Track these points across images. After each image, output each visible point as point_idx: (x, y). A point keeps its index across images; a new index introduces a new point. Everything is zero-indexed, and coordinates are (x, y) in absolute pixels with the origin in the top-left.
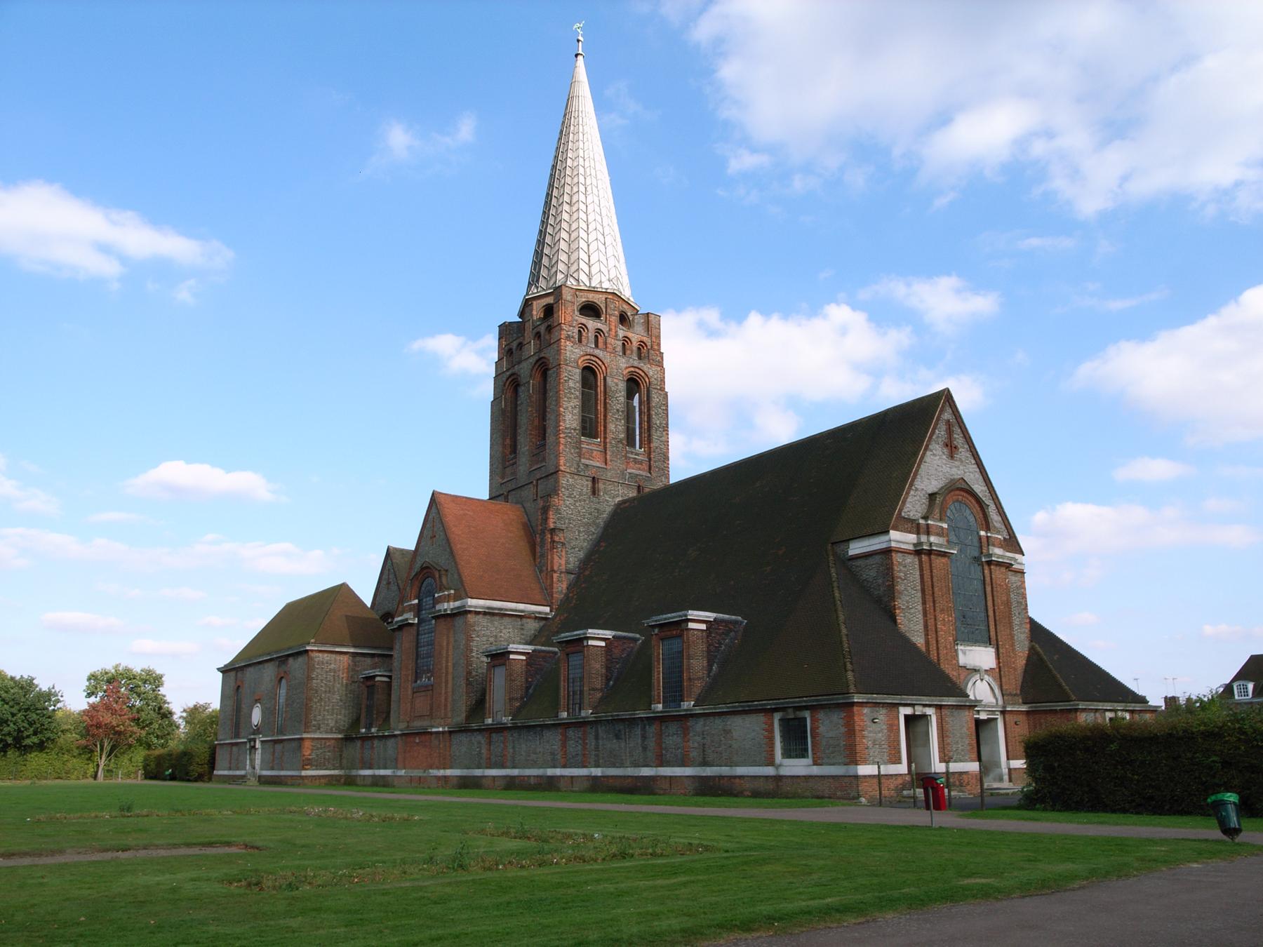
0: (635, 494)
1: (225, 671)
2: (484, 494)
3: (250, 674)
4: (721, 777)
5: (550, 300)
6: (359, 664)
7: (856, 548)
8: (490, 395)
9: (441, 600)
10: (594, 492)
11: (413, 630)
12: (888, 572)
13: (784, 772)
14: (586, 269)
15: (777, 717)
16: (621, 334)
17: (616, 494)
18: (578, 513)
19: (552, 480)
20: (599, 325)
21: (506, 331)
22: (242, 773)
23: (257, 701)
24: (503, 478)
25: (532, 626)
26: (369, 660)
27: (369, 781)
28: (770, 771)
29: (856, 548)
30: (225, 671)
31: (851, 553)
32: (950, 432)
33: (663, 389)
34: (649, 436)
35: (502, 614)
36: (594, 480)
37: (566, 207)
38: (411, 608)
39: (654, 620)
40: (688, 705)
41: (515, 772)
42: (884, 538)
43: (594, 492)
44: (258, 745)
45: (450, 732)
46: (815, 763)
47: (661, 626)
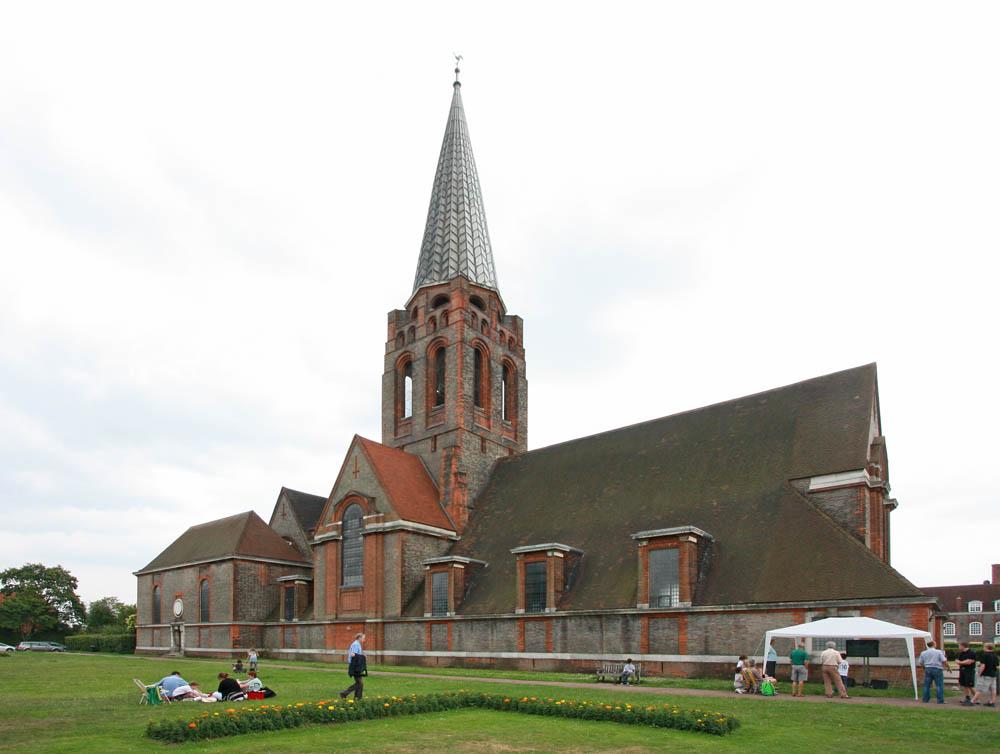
1: (140, 575)
3: (169, 579)
5: (442, 291)
6: (262, 571)
7: (816, 484)
9: (368, 521)
10: (483, 449)
12: (860, 501)
14: (473, 268)
16: (499, 328)
19: (452, 436)
20: (485, 317)
22: (167, 649)
23: (177, 597)
24: (396, 435)
25: (445, 545)
26: (280, 569)
27: (293, 657)
29: (816, 484)
30: (140, 575)
31: (811, 488)
33: (524, 378)
34: (517, 412)
35: (426, 535)
36: (483, 440)
37: (454, 214)
39: (643, 534)
41: (463, 654)
43: (483, 449)
44: (182, 629)
45: (384, 623)
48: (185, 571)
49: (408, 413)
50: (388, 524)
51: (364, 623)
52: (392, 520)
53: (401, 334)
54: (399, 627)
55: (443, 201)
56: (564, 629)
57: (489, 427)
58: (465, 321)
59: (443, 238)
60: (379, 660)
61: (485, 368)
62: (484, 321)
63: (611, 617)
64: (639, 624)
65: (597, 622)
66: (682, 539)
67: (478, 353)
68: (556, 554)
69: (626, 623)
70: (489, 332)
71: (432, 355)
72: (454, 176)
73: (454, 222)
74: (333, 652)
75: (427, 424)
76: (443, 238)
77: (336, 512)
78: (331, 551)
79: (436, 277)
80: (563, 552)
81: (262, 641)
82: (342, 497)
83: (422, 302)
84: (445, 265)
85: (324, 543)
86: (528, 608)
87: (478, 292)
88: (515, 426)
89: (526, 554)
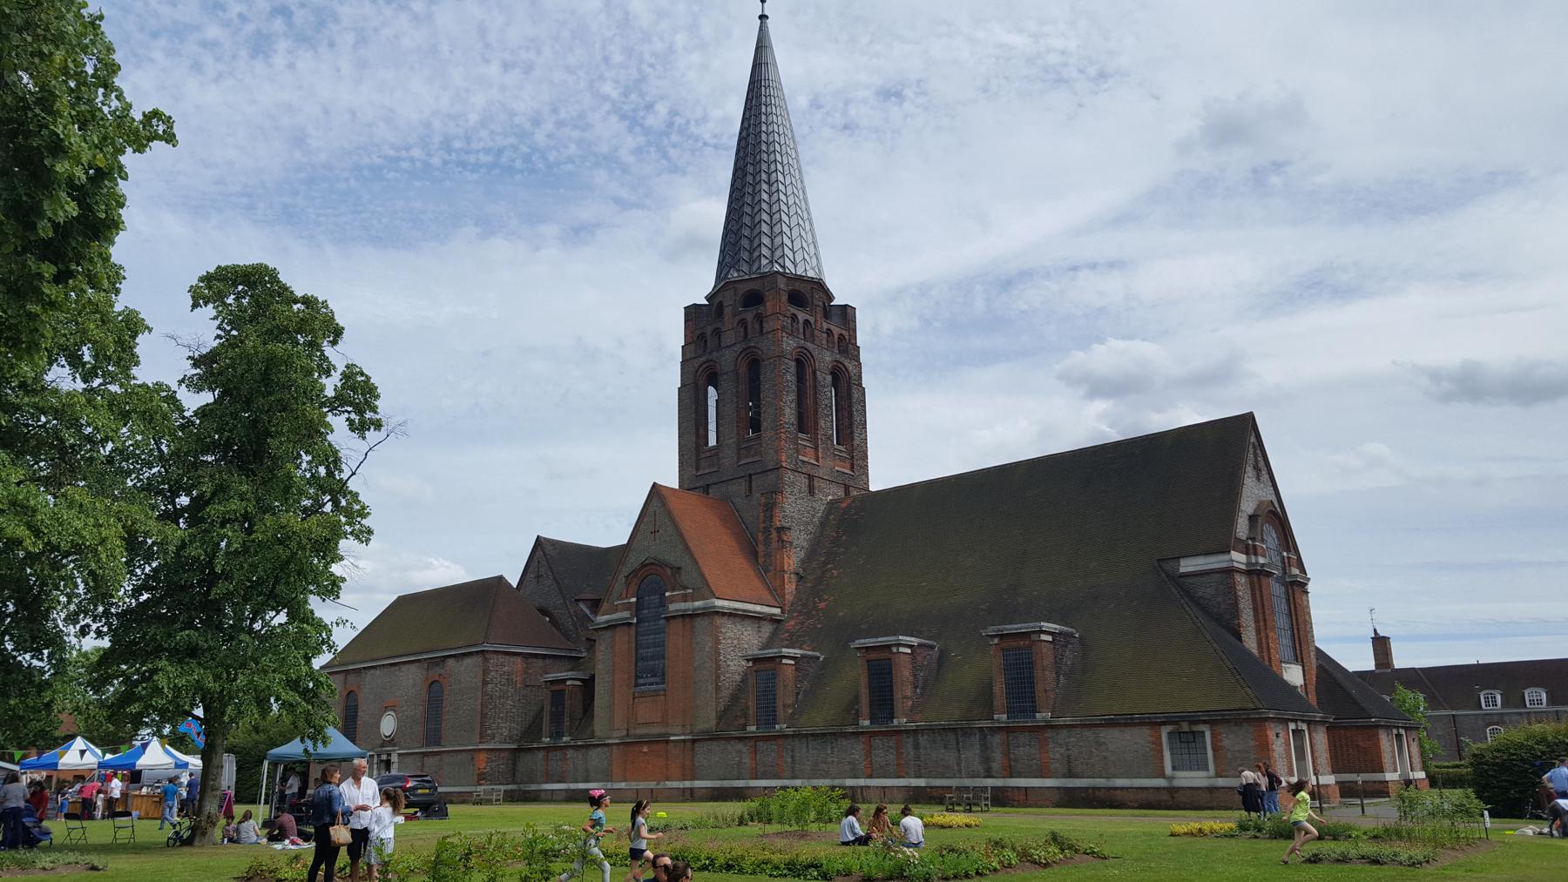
0: (841, 493)
2: (676, 486)
4: (1095, 789)
7: (1188, 565)
8: (677, 382)
9: (672, 600)
11: (633, 630)
12: (1232, 589)
13: (1177, 783)
14: (790, 255)
15: (1165, 732)
16: (825, 326)
17: (830, 493)
18: (799, 512)
21: (692, 313)
24: (697, 469)
26: (540, 663)
28: (1161, 782)
29: (1188, 565)
31: (1182, 570)
32: (1256, 456)
33: (860, 385)
36: (811, 478)
37: (765, 186)
38: (628, 607)
40: (1043, 716)
42: (1226, 557)
44: (394, 758)
45: (694, 741)
46: (1218, 775)
47: (1002, 637)
48: (404, 668)
49: (712, 442)
50: (697, 604)
51: (667, 742)
52: (704, 599)
53: (702, 336)
54: (714, 746)
55: (750, 169)
56: (916, 746)
57: (852, 469)
58: (783, 329)
59: (753, 218)
60: (688, 793)
61: (809, 376)
62: (807, 322)
63: (967, 732)
64: (997, 739)
65: (952, 736)
66: (1034, 637)
67: (800, 364)
68: (902, 650)
69: (983, 738)
70: (813, 335)
71: (743, 369)
72: (764, 137)
73: (765, 196)
74: (623, 785)
75: (739, 459)
76: (753, 218)
77: (628, 585)
78: (624, 641)
79: (745, 268)
80: (911, 647)
81: (514, 771)
82: (636, 565)
83: (728, 299)
84: (756, 254)
85: (612, 627)
86: (1010, 712)
87: (797, 285)
88: (851, 452)
89: (868, 648)
